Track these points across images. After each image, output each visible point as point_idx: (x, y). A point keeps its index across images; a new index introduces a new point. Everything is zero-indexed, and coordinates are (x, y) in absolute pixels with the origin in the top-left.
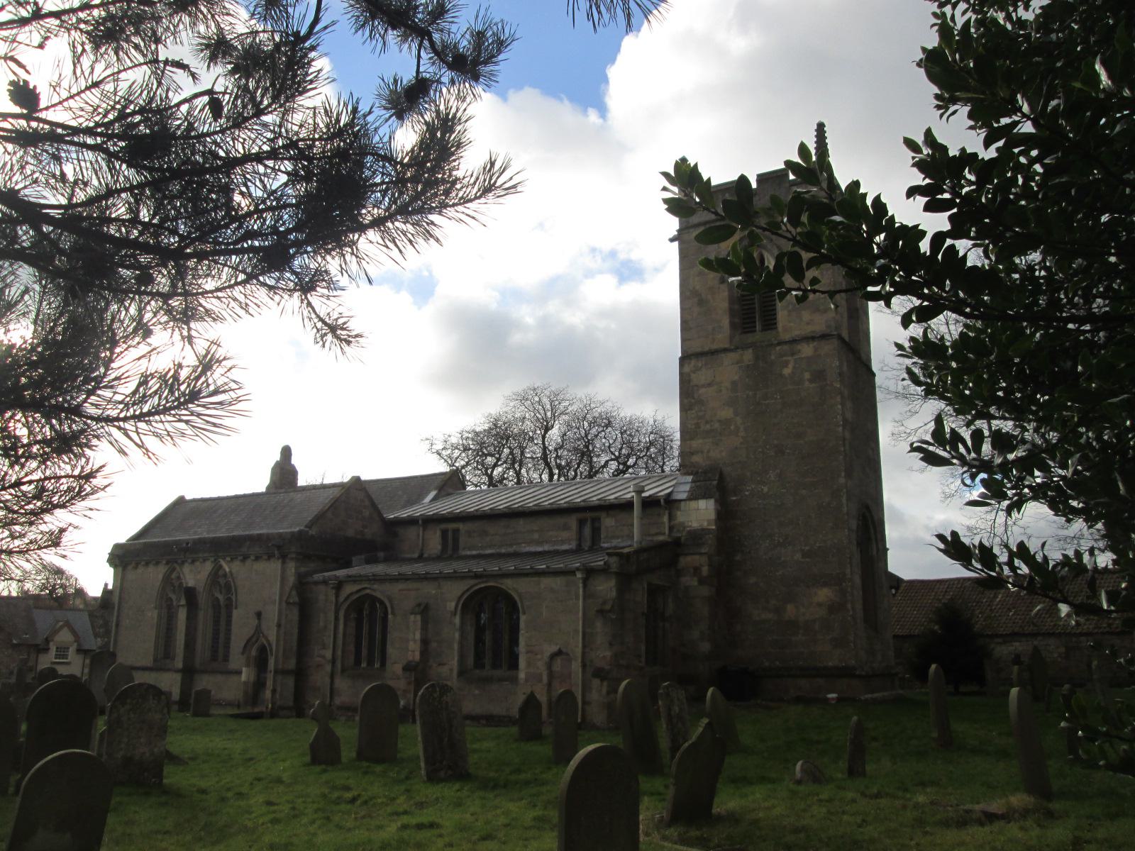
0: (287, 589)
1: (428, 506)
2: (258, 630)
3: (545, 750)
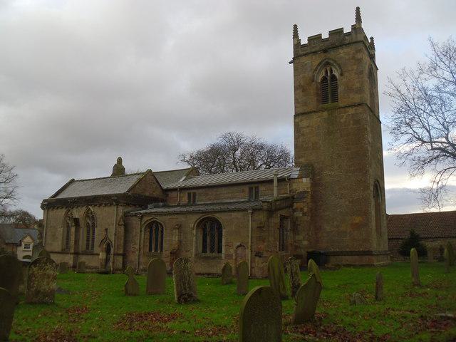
0: (119, 219)
1: (181, 182)
2: (106, 236)
3: (234, 288)
